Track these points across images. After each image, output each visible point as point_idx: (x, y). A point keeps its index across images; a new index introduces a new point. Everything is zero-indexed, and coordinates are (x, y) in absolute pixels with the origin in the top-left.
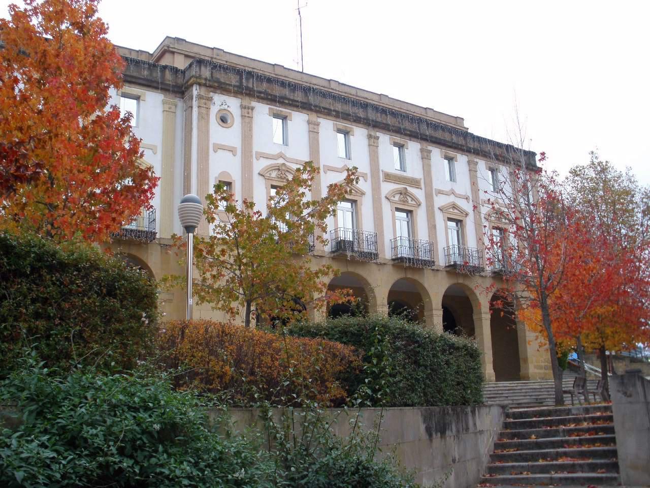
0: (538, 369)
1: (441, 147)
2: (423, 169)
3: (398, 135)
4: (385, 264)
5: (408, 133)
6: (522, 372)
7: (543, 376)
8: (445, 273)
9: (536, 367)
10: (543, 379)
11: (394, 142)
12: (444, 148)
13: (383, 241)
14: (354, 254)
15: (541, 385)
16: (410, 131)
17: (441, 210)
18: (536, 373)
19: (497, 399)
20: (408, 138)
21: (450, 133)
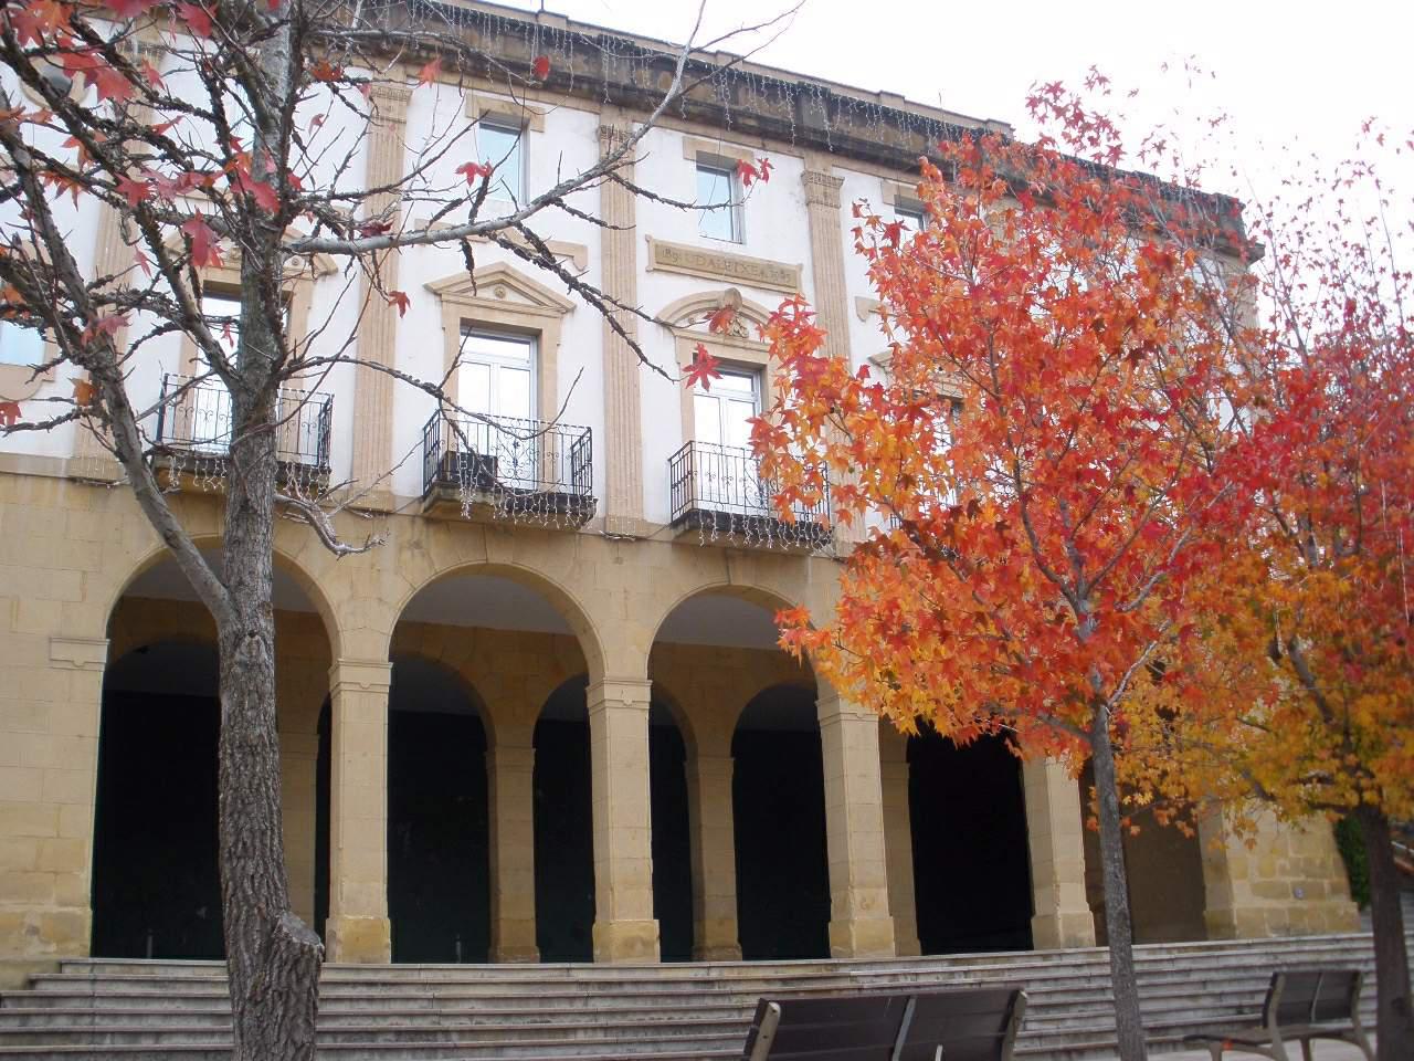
0: (1266, 896)
1: (884, 172)
2: (812, 237)
3: (717, 132)
4: (639, 539)
5: (752, 123)
6: (1211, 909)
7: (1287, 920)
8: (668, 547)
9: (1259, 890)
10: (1287, 930)
11: (699, 153)
12: (893, 174)
13: (638, 465)
14: (491, 500)
15: (1275, 955)
16: (758, 118)
17: (436, 293)
18: (1260, 910)
19: (1074, 1012)
20: (757, 141)
21: (941, 136)
